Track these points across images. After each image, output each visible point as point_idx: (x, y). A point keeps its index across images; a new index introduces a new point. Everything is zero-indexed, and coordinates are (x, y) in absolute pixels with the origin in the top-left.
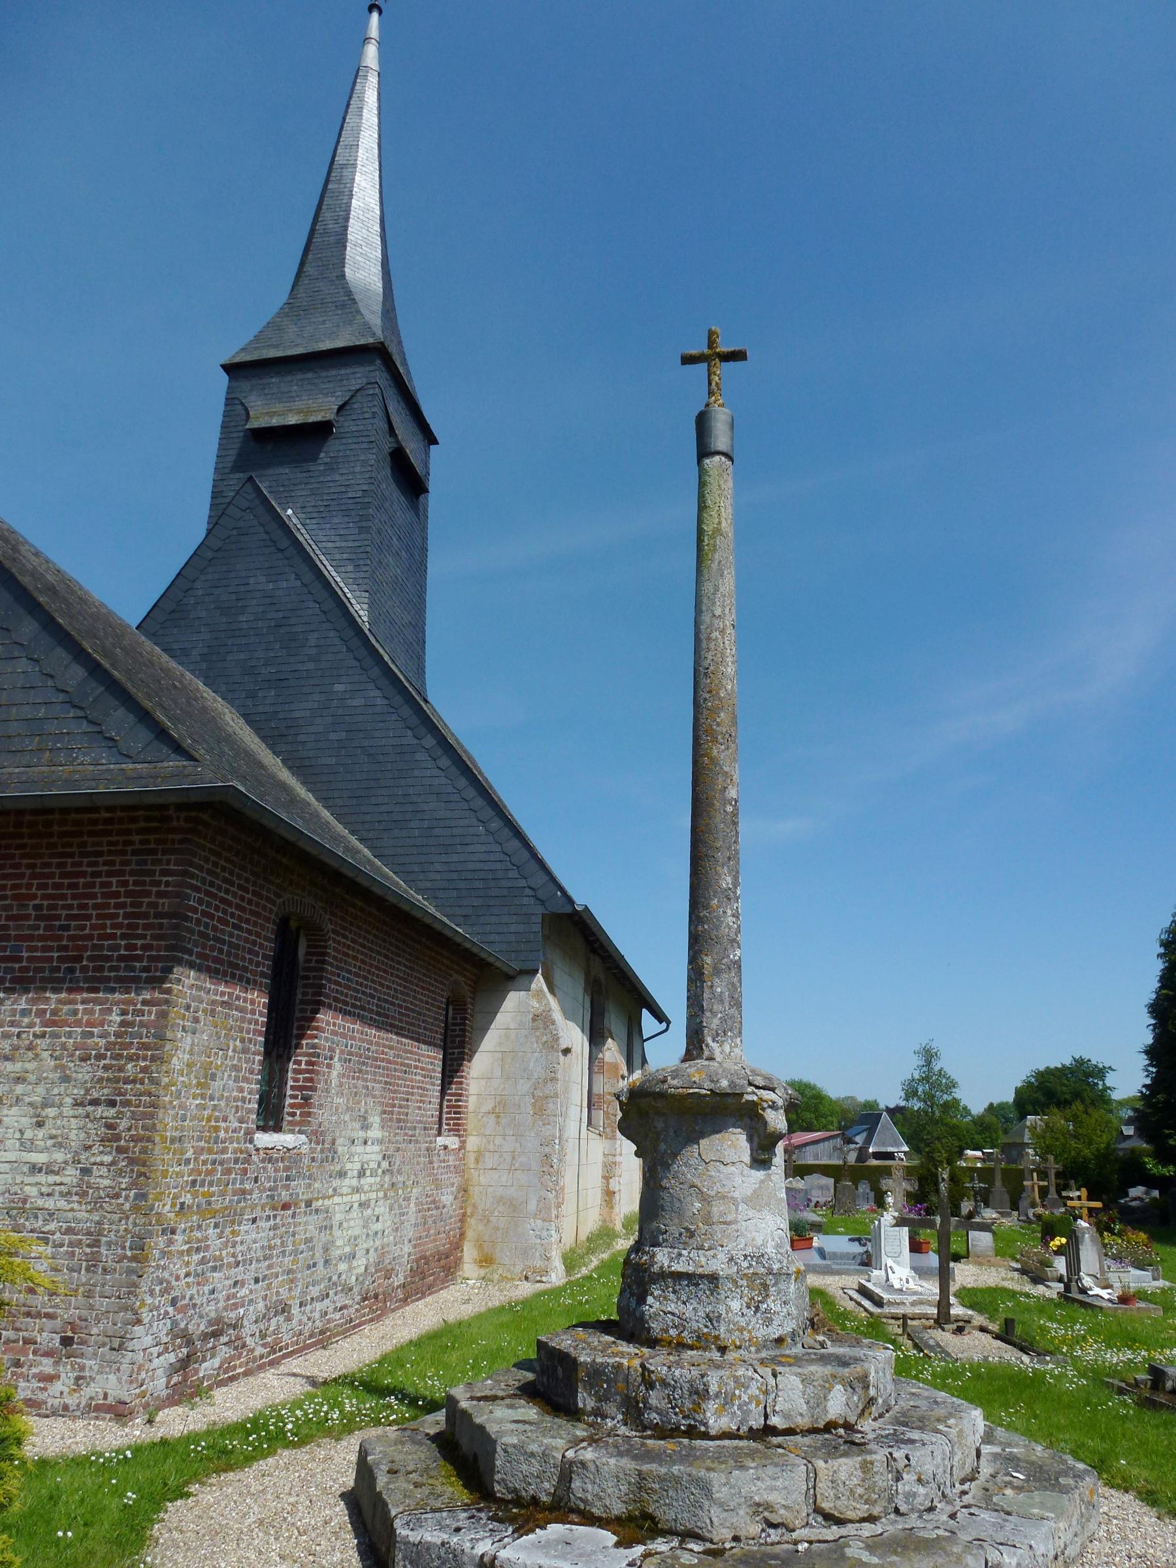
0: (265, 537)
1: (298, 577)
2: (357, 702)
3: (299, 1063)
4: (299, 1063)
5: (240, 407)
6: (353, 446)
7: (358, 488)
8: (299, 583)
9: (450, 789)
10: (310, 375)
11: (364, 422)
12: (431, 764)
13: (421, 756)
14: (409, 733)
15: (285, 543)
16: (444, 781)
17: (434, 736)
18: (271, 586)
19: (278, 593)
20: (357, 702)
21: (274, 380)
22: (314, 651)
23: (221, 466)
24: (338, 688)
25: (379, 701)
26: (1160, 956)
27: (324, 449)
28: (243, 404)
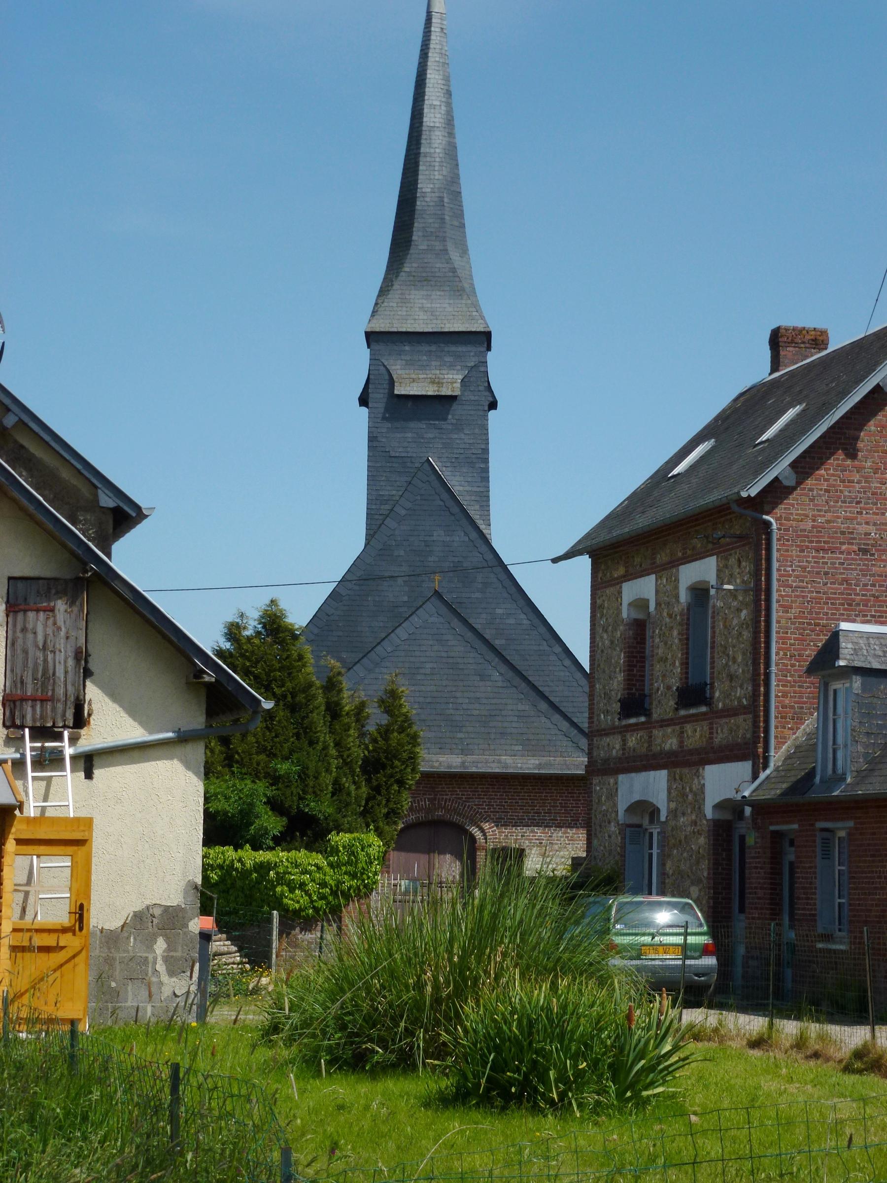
0: (442, 503)
1: (466, 534)
2: (512, 621)
3: (815, 645)
4: (815, 645)
5: (382, 368)
6: (472, 412)
7: (479, 446)
8: (467, 539)
9: (571, 679)
10: (433, 348)
11: (479, 394)
12: (559, 663)
13: (553, 658)
14: (545, 643)
15: (456, 510)
16: (568, 674)
17: (561, 647)
18: (448, 539)
19: (389, 488)
20: (512, 621)
21: (407, 348)
22: (480, 586)
23: (373, 415)
24: (499, 611)
25: (526, 622)
26: (233, 632)
27: (451, 412)
28: (385, 366)
